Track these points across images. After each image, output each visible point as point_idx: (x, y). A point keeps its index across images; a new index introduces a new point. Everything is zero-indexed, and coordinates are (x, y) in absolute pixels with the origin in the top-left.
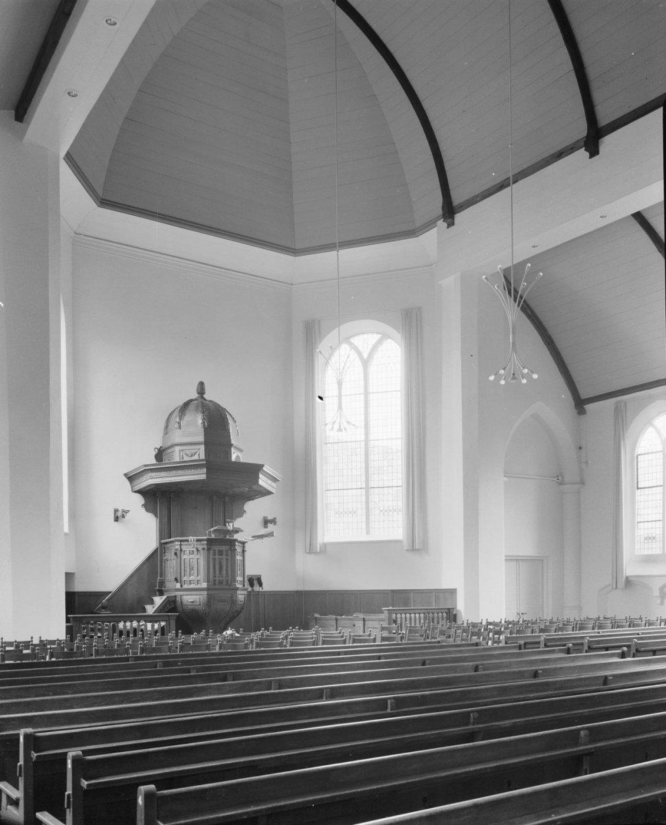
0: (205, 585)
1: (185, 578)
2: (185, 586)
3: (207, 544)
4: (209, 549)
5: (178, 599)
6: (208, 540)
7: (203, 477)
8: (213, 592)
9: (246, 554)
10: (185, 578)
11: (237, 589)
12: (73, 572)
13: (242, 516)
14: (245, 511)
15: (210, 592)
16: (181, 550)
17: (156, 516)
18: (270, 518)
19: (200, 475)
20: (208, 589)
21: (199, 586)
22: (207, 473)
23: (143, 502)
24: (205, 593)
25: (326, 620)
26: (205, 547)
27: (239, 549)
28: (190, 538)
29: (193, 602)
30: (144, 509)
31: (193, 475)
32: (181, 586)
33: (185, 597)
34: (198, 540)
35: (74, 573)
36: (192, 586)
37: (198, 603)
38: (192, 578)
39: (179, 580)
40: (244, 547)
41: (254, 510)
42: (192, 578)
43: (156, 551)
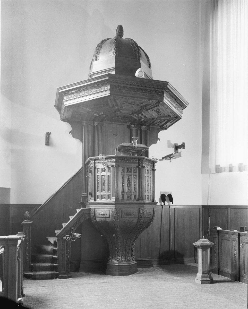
0: (113, 199)
1: (98, 193)
2: (98, 200)
3: (116, 162)
4: (118, 166)
5: (92, 212)
6: (116, 158)
7: (108, 93)
8: (121, 206)
9: (156, 172)
10: (98, 193)
11: (144, 203)
12: (8, 187)
13: (156, 143)
14: (158, 139)
15: (118, 206)
16: (95, 168)
17: (82, 141)
18: (180, 144)
19: (109, 95)
20: (115, 203)
21: (109, 200)
22: (111, 90)
23: (71, 129)
24: (113, 206)
25: (228, 233)
26: (114, 164)
27: (147, 167)
28: (100, 157)
29: (103, 215)
30: (71, 135)
31: (102, 91)
32: (95, 200)
33: (97, 210)
34: (107, 158)
35: (10, 188)
36: (104, 200)
37: (108, 216)
38: (104, 193)
39: (93, 194)
40: (153, 166)
41: (168, 137)
42: (104, 193)
43: (82, 169)
